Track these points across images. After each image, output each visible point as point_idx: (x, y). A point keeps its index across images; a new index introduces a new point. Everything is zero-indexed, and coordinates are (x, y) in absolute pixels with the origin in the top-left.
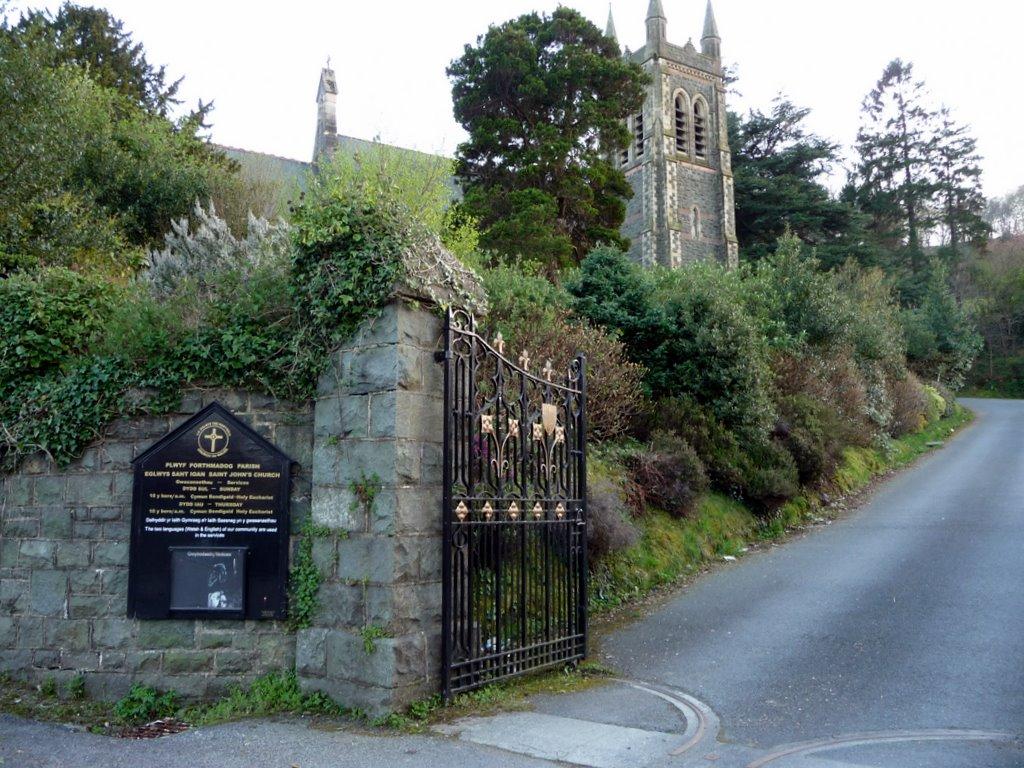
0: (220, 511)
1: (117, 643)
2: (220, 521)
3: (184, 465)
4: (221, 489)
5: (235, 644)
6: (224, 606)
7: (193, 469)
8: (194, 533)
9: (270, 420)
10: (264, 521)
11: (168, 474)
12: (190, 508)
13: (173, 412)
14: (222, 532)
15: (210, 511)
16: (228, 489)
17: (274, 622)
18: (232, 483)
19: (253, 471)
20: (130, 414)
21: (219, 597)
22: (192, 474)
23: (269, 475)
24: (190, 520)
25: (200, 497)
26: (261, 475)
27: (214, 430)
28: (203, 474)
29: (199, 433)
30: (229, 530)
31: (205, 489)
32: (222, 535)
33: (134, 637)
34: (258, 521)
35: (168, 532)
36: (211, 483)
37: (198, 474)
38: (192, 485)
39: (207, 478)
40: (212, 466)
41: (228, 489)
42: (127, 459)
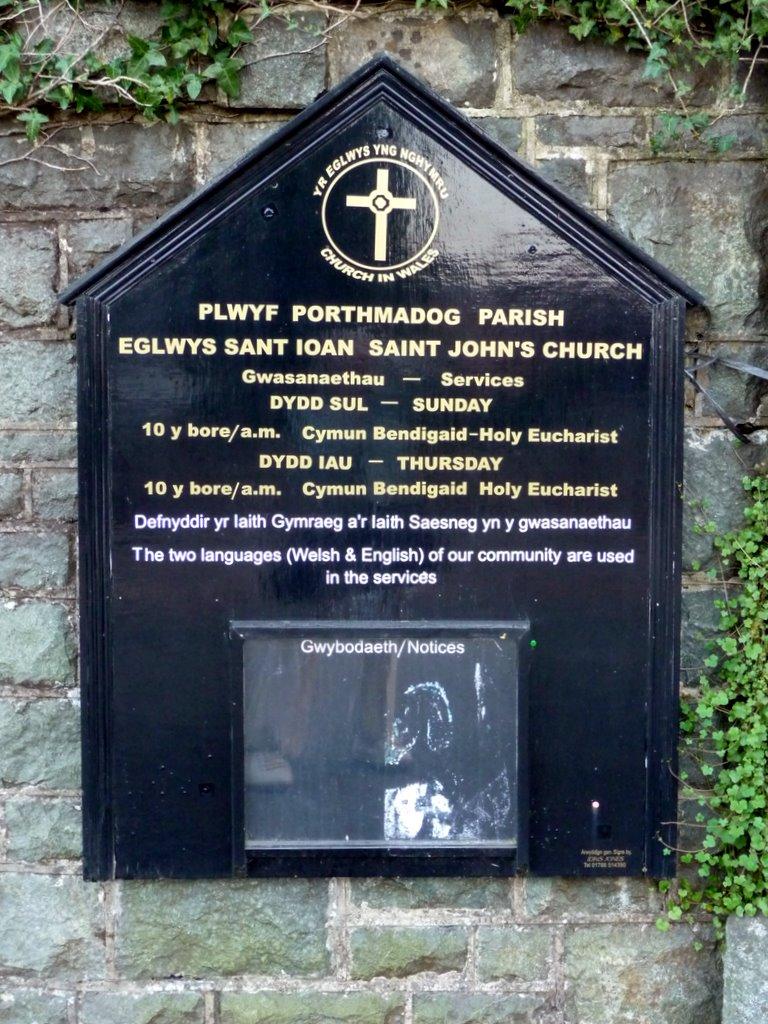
0: (417, 489)
1: (42, 956)
2: (418, 523)
3: (271, 311)
4: (419, 405)
5: (476, 958)
6: (442, 832)
7: (307, 329)
8: (322, 567)
9: (589, 141)
10: (584, 524)
11: (210, 346)
12: (301, 475)
13: (218, 106)
14: (428, 566)
15: (379, 488)
16: (446, 405)
17: (623, 883)
18: (459, 381)
19: (538, 335)
20: (47, 108)
21: (423, 802)
22: (303, 347)
23: (601, 350)
24: (306, 522)
25: (335, 434)
26: (569, 350)
27: (383, 176)
28: (347, 348)
29: (323, 188)
30: (455, 556)
31: (358, 405)
32: (428, 578)
33: (102, 935)
34: (565, 524)
35: (220, 564)
36: (380, 381)
37: (328, 348)
38: (309, 390)
39: (361, 362)
40: (383, 315)
41: (446, 405)
42: (45, 301)
